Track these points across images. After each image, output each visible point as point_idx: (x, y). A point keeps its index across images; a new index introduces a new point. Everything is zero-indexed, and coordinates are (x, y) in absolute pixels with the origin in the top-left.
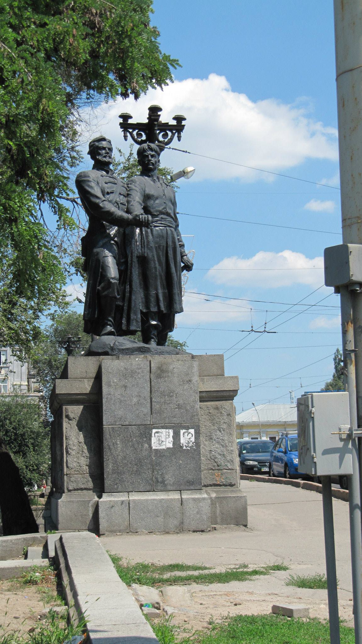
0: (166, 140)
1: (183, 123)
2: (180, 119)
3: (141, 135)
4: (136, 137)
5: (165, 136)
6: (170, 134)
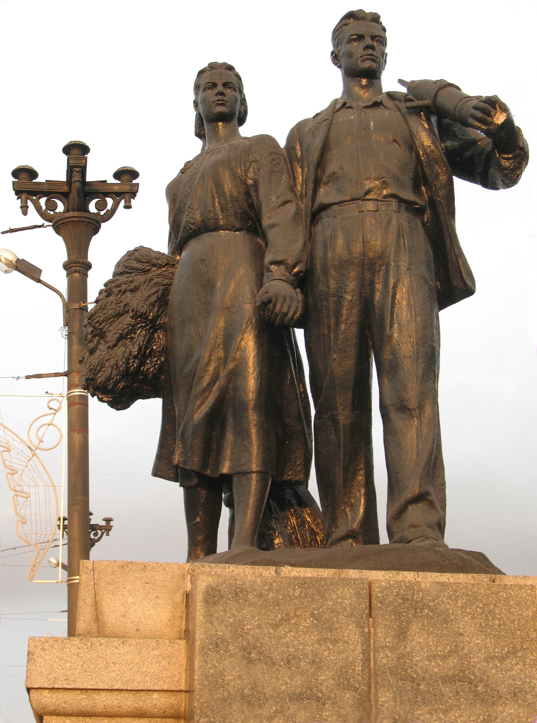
0: (96, 538)
1: (112, 523)
2: (108, 520)
3: (55, 206)
4: (44, 208)
5: (95, 535)
6: (100, 533)
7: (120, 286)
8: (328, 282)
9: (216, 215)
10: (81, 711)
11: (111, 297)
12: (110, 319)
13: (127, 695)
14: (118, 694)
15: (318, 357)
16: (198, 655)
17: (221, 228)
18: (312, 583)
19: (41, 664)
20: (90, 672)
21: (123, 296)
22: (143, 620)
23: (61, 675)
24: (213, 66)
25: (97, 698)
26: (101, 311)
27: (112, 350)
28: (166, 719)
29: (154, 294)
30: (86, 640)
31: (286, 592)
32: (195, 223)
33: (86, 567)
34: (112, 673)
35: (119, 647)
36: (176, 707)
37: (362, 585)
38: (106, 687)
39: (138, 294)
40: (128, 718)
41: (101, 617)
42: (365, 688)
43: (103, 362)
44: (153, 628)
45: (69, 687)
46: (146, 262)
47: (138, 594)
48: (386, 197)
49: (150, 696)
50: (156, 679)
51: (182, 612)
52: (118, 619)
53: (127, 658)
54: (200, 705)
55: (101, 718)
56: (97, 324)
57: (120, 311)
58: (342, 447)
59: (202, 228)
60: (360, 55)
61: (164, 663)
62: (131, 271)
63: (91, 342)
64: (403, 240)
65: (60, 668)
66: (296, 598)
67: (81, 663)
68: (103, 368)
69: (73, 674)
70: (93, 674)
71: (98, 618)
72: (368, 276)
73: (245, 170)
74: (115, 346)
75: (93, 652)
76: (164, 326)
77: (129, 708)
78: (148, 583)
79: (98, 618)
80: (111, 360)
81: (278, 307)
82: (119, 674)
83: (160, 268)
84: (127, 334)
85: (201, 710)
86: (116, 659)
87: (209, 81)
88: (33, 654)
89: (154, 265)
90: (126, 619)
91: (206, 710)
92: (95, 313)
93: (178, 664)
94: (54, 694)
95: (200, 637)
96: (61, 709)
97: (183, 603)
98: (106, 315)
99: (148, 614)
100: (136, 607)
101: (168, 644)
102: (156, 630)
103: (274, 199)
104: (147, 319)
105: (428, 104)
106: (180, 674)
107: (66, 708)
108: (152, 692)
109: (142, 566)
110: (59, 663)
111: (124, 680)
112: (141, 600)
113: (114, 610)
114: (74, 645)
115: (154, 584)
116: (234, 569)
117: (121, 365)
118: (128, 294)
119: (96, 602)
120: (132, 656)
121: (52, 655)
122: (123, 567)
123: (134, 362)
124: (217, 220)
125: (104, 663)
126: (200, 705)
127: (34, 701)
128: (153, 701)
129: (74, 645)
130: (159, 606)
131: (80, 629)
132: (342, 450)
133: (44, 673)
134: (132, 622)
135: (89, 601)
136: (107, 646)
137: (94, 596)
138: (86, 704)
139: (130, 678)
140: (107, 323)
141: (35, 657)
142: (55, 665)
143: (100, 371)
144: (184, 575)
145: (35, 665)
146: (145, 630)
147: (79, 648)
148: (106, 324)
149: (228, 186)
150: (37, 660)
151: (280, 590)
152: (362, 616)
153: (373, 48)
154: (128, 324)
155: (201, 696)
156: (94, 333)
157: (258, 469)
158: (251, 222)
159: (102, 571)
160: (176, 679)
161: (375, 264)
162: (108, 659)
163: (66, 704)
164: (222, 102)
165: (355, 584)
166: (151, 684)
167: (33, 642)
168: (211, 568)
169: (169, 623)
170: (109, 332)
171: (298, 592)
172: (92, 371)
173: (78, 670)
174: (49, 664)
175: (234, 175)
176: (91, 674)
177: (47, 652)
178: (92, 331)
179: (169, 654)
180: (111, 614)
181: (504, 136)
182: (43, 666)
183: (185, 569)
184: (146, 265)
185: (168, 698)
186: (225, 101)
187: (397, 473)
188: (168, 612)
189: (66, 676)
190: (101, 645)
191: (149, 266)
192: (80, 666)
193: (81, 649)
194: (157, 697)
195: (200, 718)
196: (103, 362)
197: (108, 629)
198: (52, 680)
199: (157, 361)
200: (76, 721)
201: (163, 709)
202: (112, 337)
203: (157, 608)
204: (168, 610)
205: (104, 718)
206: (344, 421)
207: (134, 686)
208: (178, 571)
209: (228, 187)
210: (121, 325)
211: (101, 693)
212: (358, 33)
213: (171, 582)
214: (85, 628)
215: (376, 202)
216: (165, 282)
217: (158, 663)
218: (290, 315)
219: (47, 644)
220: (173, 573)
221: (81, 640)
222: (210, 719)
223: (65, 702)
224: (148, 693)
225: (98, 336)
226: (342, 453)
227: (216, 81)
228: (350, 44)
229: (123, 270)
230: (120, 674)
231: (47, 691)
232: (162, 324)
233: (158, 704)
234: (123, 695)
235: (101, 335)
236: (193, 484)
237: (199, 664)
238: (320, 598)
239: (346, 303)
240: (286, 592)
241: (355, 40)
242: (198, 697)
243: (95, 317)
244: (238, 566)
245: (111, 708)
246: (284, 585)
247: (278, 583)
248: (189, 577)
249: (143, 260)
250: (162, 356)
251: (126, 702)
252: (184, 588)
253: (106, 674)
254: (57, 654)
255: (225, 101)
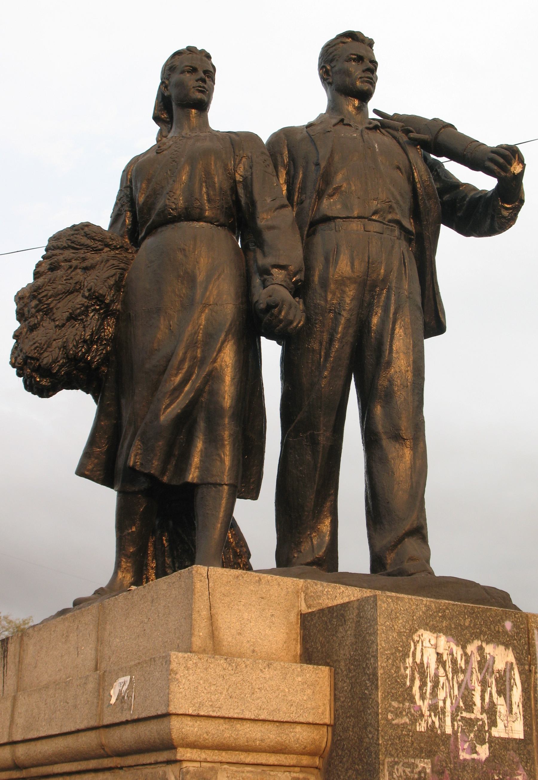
7: (70, 261)
8: (326, 296)
9: (202, 204)
10: (222, 743)
11: (59, 271)
12: (59, 295)
13: (270, 726)
14: (262, 726)
15: (304, 372)
16: (381, 685)
17: (204, 220)
18: (479, 613)
19: (185, 686)
20: (235, 698)
21: (73, 273)
22: (259, 640)
23: (206, 699)
24: (191, 50)
25: (240, 729)
26: (50, 285)
27: (59, 329)
28: (301, 756)
29: (112, 276)
30: (231, 660)
31: (458, 621)
32: (176, 209)
33: (201, 574)
34: (258, 701)
35: (264, 670)
36: (317, 743)
37: (521, 619)
38: (253, 717)
39: (93, 274)
40: (265, 754)
41: (216, 633)
42: (528, 730)
43: (50, 342)
44: (269, 650)
45: (214, 714)
46: (99, 241)
47: (253, 609)
48: (390, 221)
49: (294, 729)
50: (301, 709)
51: (297, 633)
52: (234, 637)
53: (273, 683)
54: (385, 743)
55: (237, 752)
56: (45, 299)
57: (70, 288)
58: (318, 469)
59: (183, 215)
60: (360, 76)
61: (309, 692)
62: (78, 247)
63: (33, 317)
64: (404, 269)
65: (205, 691)
66: (467, 628)
67: (226, 687)
68: (50, 348)
69: (218, 700)
70: (239, 701)
71: (213, 634)
72: (367, 297)
73: (235, 164)
74: (63, 325)
75: (238, 675)
76: (116, 313)
77: (271, 741)
78: (263, 598)
79: (213, 634)
80: (59, 340)
81: (283, 314)
82: (265, 702)
83: (113, 249)
84: (79, 315)
85: (386, 748)
86: (261, 684)
87: (190, 65)
88: (176, 673)
89: (107, 245)
90: (242, 638)
91: (391, 749)
92: (43, 285)
93: (322, 694)
94: (196, 722)
95: (382, 665)
96: (201, 740)
97: (297, 623)
98: (56, 290)
99: (263, 633)
100: (252, 624)
101: (312, 670)
102: (272, 653)
103: (269, 200)
104: (103, 302)
105: (428, 139)
106: (324, 705)
107: (207, 739)
108: (295, 725)
109: (257, 578)
110: (203, 685)
111: (269, 709)
112: (257, 616)
113: (230, 626)
114: (219, 665)
115: (269, 600)
116: (344, 590)
117: (72, 348)
118: (79, 271)
119: (211, 616)
120: (277, 682)
121: (196, 676)
122: (238, 577)
123: (83, 347)
124: (202, 210)
125: (250, 688)
126: (385, 743)
127: (175, 730)
128: (296, 735)
129: (219, 665)
130: (274, 625)
131: (195, 646)
132: (318, 472)
133: (188, 696)
134: (248, 641)
135: (205, 613)
136: (252, 669)
137: (209, 608)
138: (229, 735)
139: (275, 707)
140: (56, 299)
141: (178, 676)
142: (199, 687)
143: (45, 351)
144: (298, 592)
145: (179, 686)
146: (261, 652)
147: (224, 669)
148: (54, 300)
149: (218, 179)
150: (181, 681)
151: (452, 618)
152: (523, 652)
153: (204, 81)
154: (81, 304)
155: (385, 733)
156: (39, 307)
157: (231, 482)
158: (232, 220)
159: (217, 580)
160: (320, 711)
161: (376, 286)
162: (254, 684)
163: (208, 735)
164: (203, 89)
165: (515, 617)
166: (297, 716)
167: (175, 658)
168: (323, 587)
169: (284, 646)
170: (57, 309)
171: (468, 622)
172: (38, 349)
173: (224, 695)
174: (193, 686)
175: (225, 168)
176: (236, 700)
177: (191, 671)
178: (37, 306)
179: (313, 682)
180: (227, 631)
181: (514, 186)
182: (187, 688)
183: (298, 586)
184: (99, 244)
185: (311, 732)
186: (206, 89)
187: (388, 502)
188: (283, 633)
189: (211, 701)
190: (246, 666)
191: (102, 245)
192: (225, 691)
193: (227, 671)
194: (300, 730)
195: (385, 758)
196: (50, 342)
197: (224, 648)
198: (197, 705)
199: (103, 350)
200: (212, 755)
201: (305, 744)
202: (61, 314)
203: (272, 628)
204: (283, 631)
205: (241, 753)
206: (325, 443)
207: (280, 717)
208: (292, 587)
209: (218, 179)
210: (71, 304)
211: (244, 723)
212: (359, 54)
213: (286, 599)
214: (200, 645)
215: (382, 224)
216: (122, 265)
217: (302, 692)
218: (295, 324)
219: (191, 662)
220: (287, 589)
221: (226, 659)
222: (394, 759)
223: (206, 732)
224: (291, 726)
225: (43, 312)
226: (317, 476)
227: (197, 66)
228: (349, 62)
229: (68, 245)
230: (266, 703)
231: (189, 718)
232: (115, 310)
233: (301, 738)
234: (266, 727)
235: (48, 312)
236: (137, 490)
237: (382, 695)
238: (487, 630)
239: (343, 321)
240: (458, 621)
241: (354, 60)
242: (382, 733)
243: (43, 290)
244: (347, 587)
245: (254, 741)
246: (456, 612)
247: (451, 611)
248: (303, 595)
249: (96, 238)
250: (109, 345)
251: (269, 735)
252: (299, 607)
253: (252, 701)
254: (202, 675)
255: (206, 89)
